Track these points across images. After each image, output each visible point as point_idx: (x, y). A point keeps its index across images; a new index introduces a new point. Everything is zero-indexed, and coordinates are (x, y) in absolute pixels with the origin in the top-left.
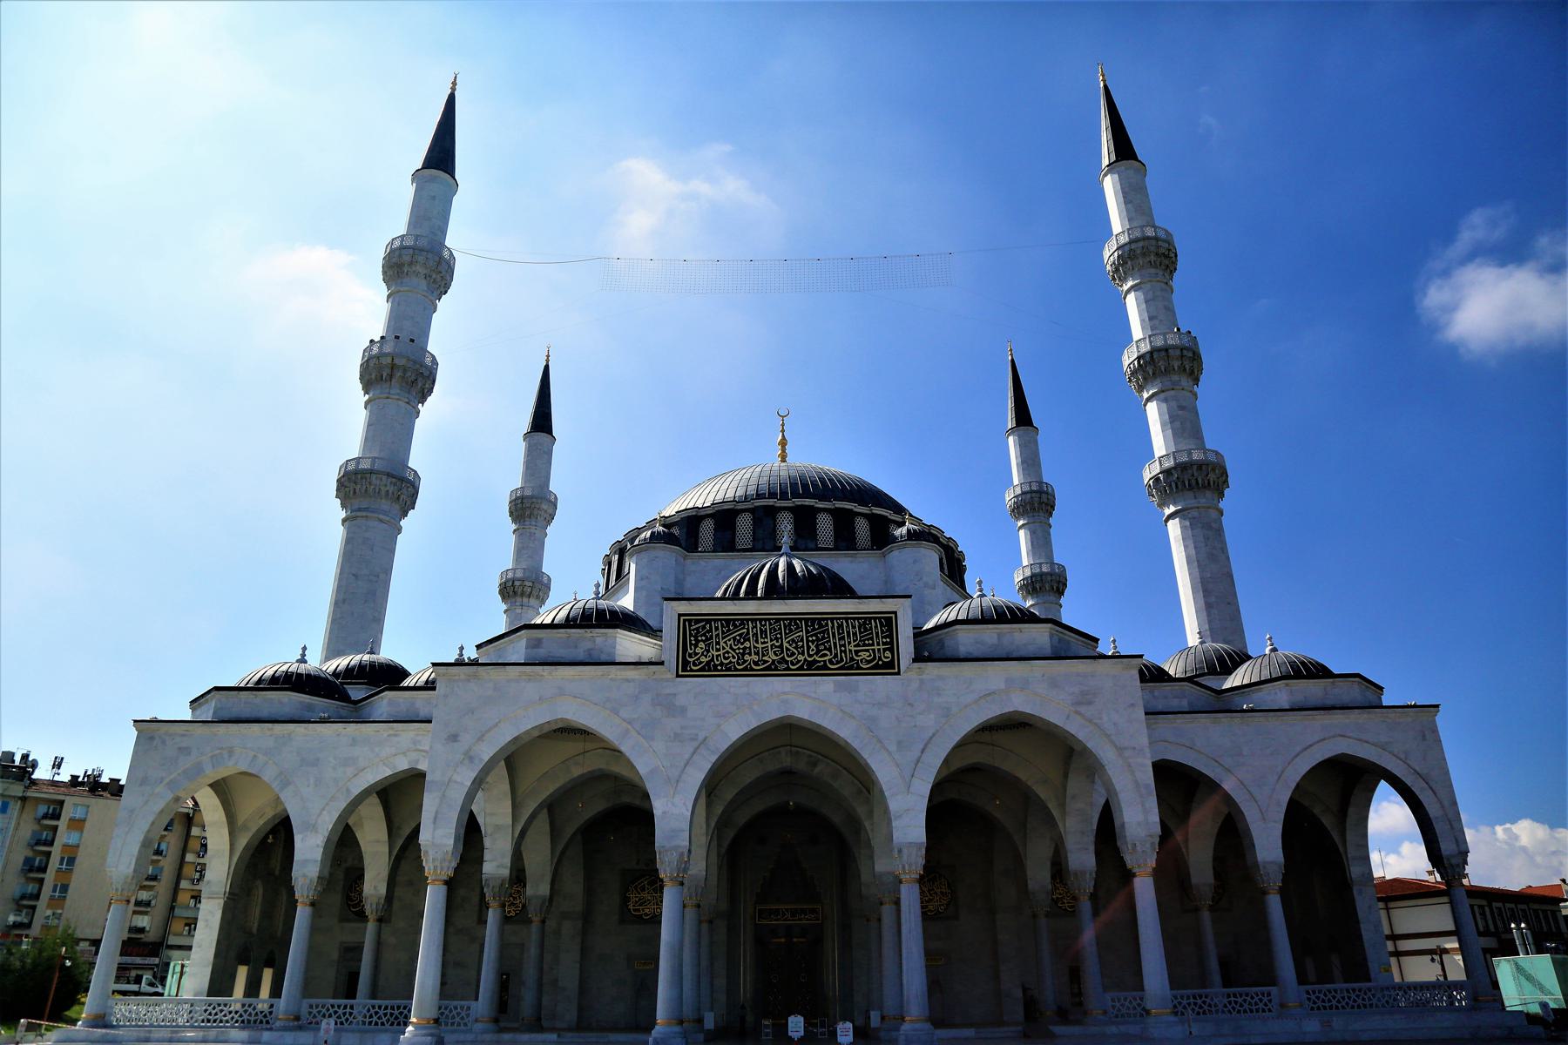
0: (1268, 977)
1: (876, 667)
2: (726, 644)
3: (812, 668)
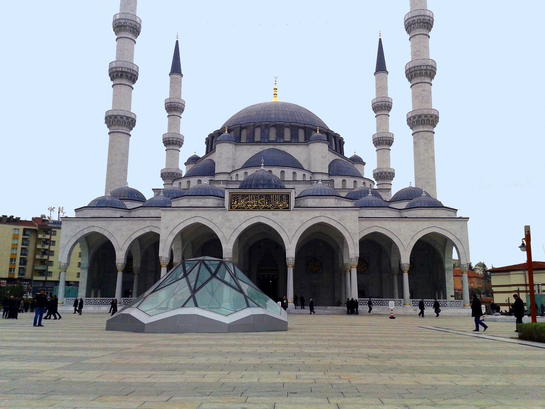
0: (26, 248)
1: (284, 209)
2: (242, 202)
3: (266, 209)
